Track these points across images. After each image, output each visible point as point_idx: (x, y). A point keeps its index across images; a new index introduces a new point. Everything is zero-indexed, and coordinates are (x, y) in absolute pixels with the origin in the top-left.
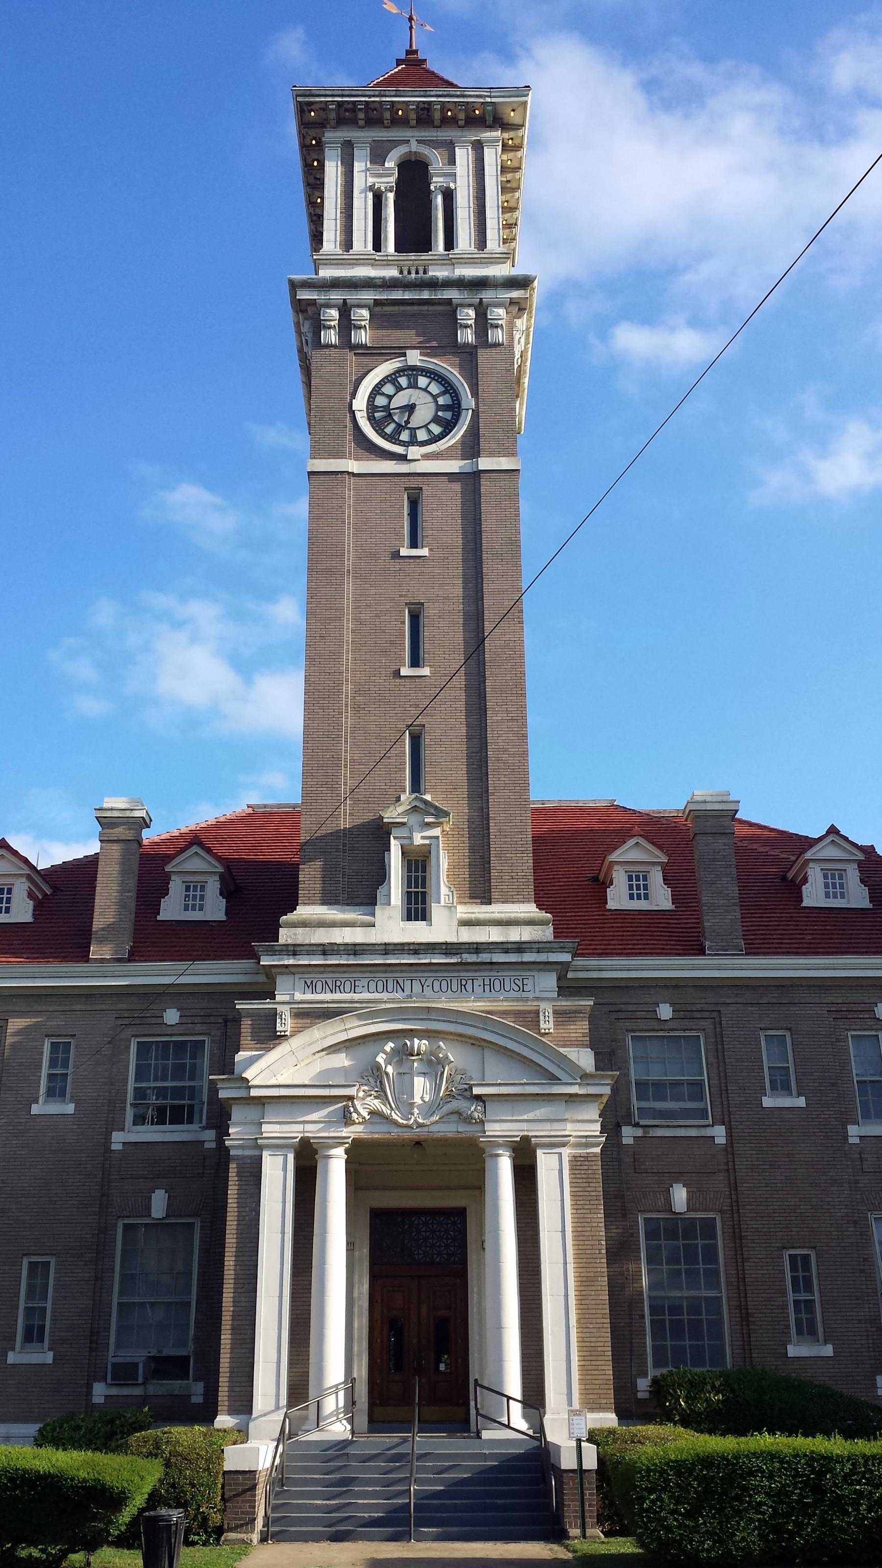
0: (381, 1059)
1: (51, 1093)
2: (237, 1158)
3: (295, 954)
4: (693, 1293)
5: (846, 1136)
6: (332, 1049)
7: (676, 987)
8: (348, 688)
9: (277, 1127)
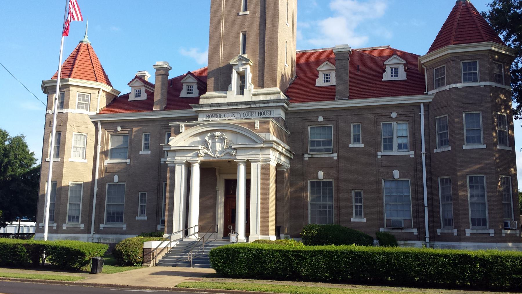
0: (207, 138)
1: (355, 141)
2: (169, 167)
3: (202, 107)
4: (324, 203)
5: (376, 156)
6: (195, 135)
7: (325, 111)
8: (223, 21)
9: (179, 158)
